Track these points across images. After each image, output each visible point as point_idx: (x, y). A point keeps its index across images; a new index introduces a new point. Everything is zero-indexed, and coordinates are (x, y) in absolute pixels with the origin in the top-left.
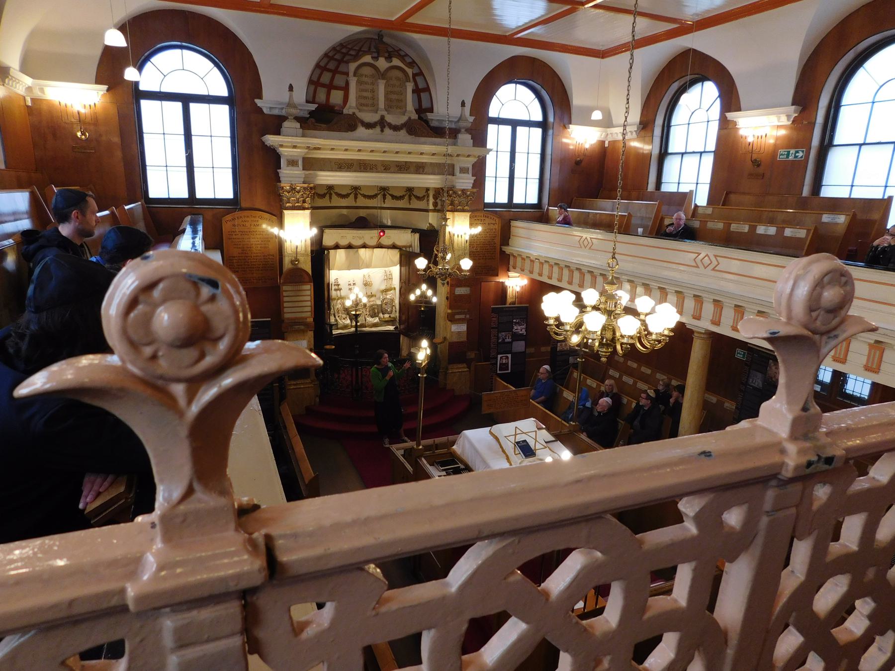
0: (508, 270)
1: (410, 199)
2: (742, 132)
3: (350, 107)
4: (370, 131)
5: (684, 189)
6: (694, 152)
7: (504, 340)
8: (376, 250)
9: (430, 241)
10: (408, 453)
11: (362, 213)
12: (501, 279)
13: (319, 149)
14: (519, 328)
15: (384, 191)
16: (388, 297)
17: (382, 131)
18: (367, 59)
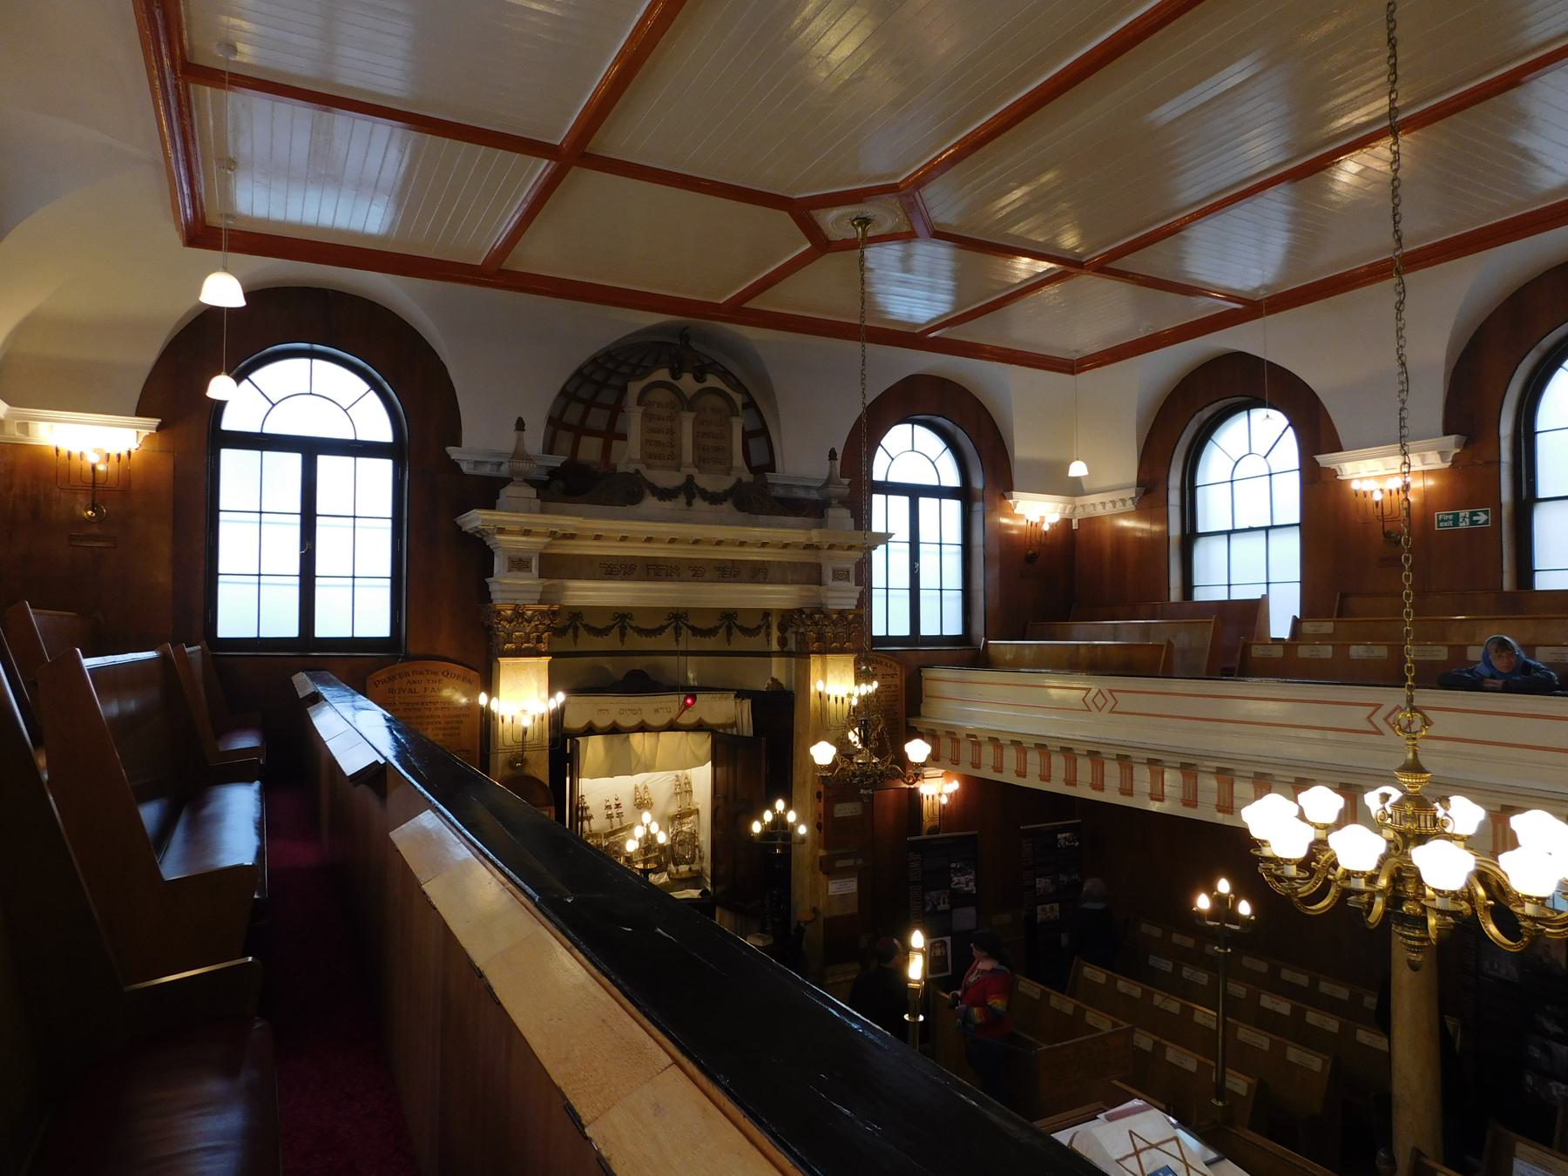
1: (729, 633)
3: (631, 460)
4: (667, 504)
5: (1239, 594)
6: (1251, 529)
7: (935, 906)
8: (667, 738)
11: (638, 663)
13: (572, 537)
14: (963, 879)
15: (678, 618)
17: (689, 504)
18: (663, 375)
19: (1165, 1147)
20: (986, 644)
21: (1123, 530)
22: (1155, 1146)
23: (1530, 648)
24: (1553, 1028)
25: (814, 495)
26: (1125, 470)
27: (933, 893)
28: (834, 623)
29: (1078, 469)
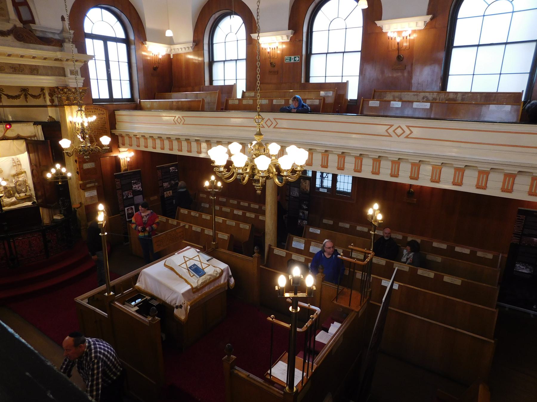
0: (119, 147)
1: (26, 98)
2: (263, 46)
5: (228, 83)
6: (231, 60)
7: (127, 196)
9: (54, 129)
10: (91, 300)
12: (114, 154)
14: (137, 186)
16: (20, 179)
19: (195, 259)
20: (140, 101)
21: (189, 59)
22: (192, 259)
23: (305, 100)
24: (305, 207)
25: (57, 37)
26: (188, 35)
27: (126, 192)
28: (74, 93)
29: (169, 33)
